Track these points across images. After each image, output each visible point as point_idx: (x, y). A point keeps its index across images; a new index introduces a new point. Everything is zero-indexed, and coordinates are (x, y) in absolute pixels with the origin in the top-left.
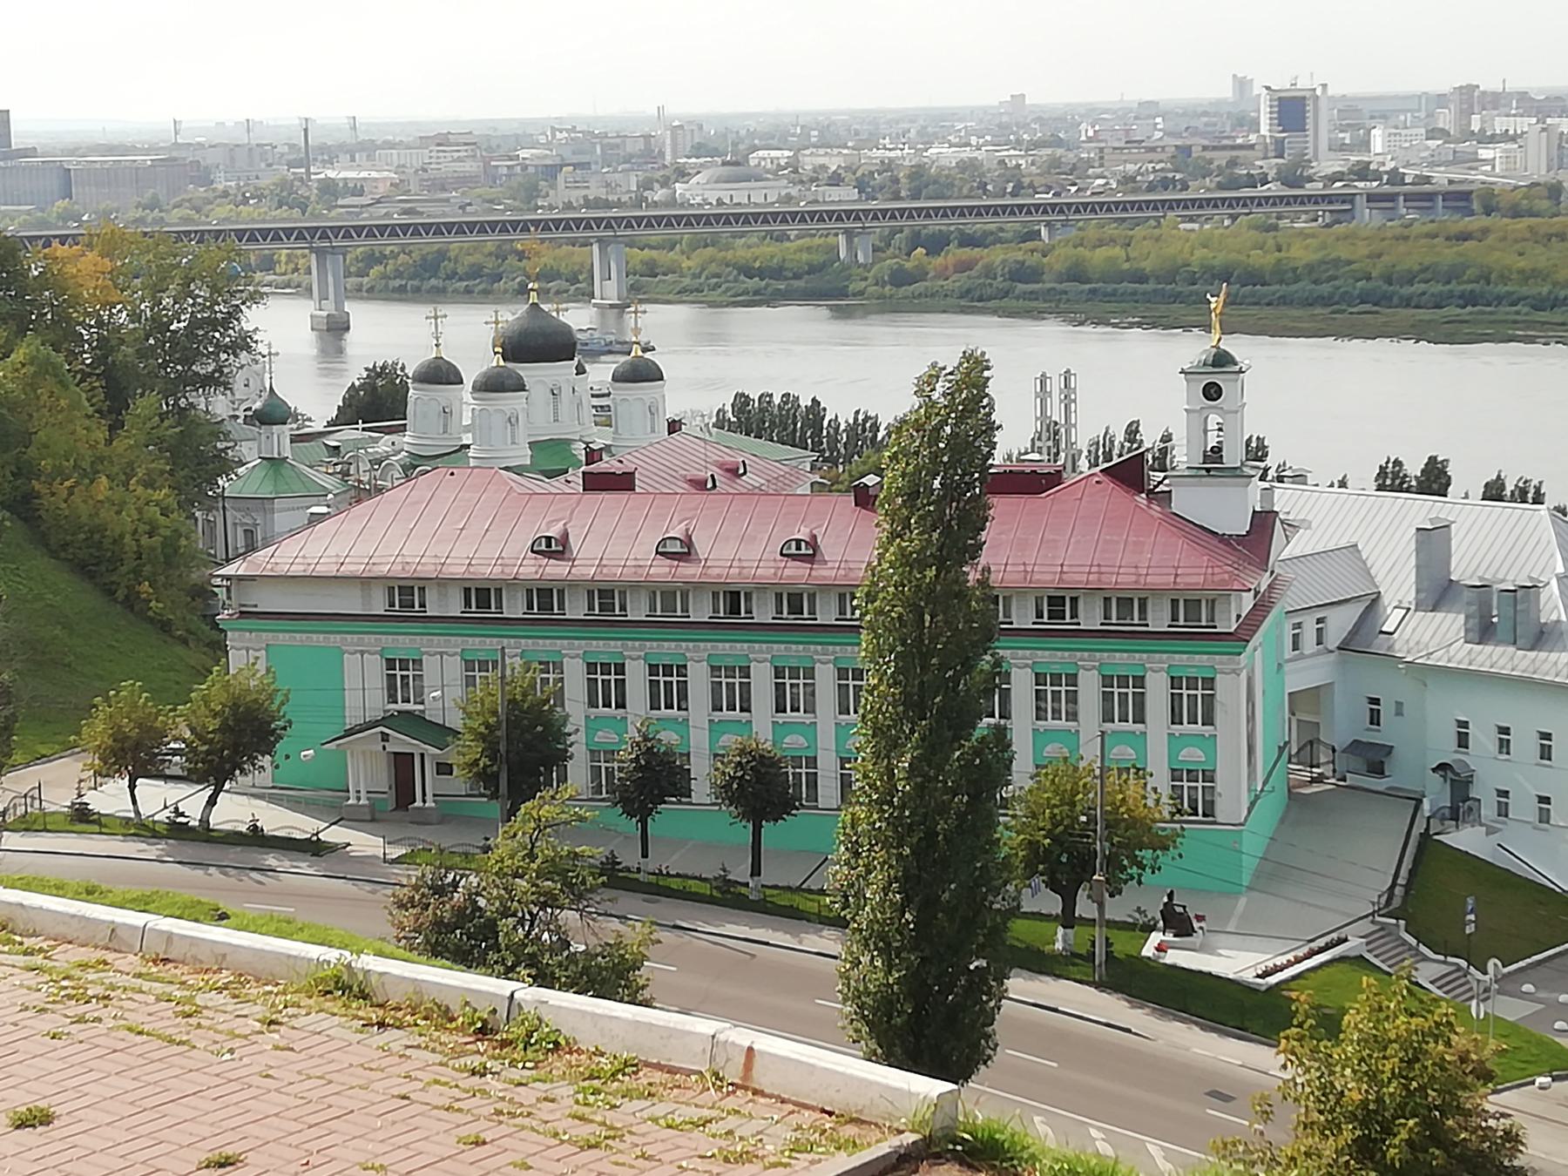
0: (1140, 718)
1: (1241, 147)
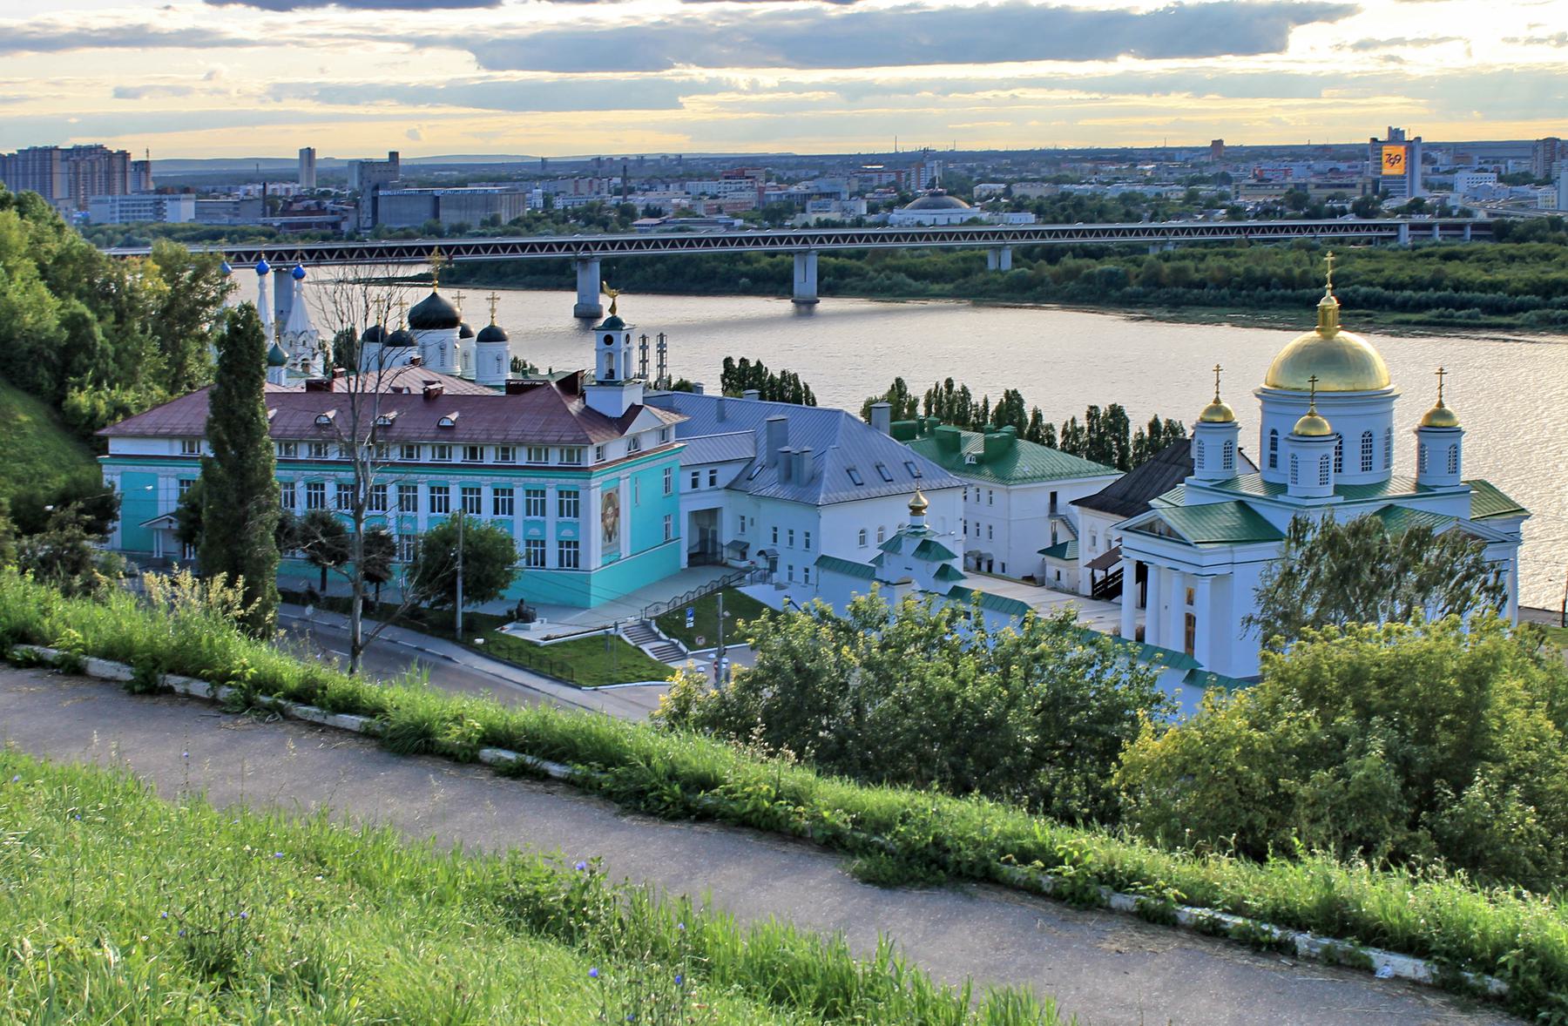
1: (1346, 186)
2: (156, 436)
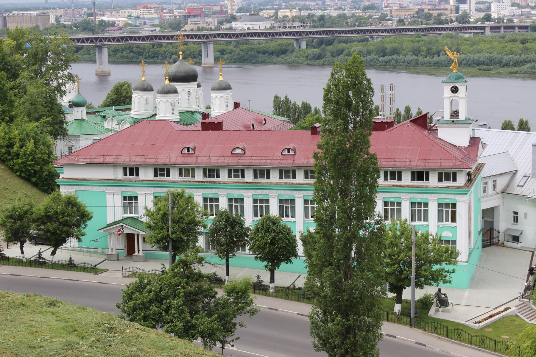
0: (426, 219)
1: (443, 9)
2: (104, 165)
